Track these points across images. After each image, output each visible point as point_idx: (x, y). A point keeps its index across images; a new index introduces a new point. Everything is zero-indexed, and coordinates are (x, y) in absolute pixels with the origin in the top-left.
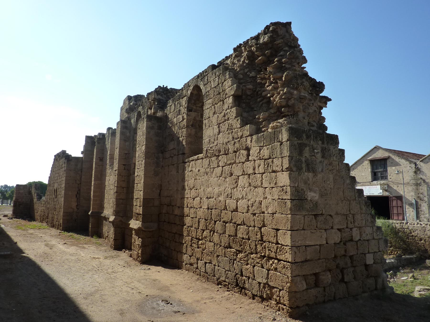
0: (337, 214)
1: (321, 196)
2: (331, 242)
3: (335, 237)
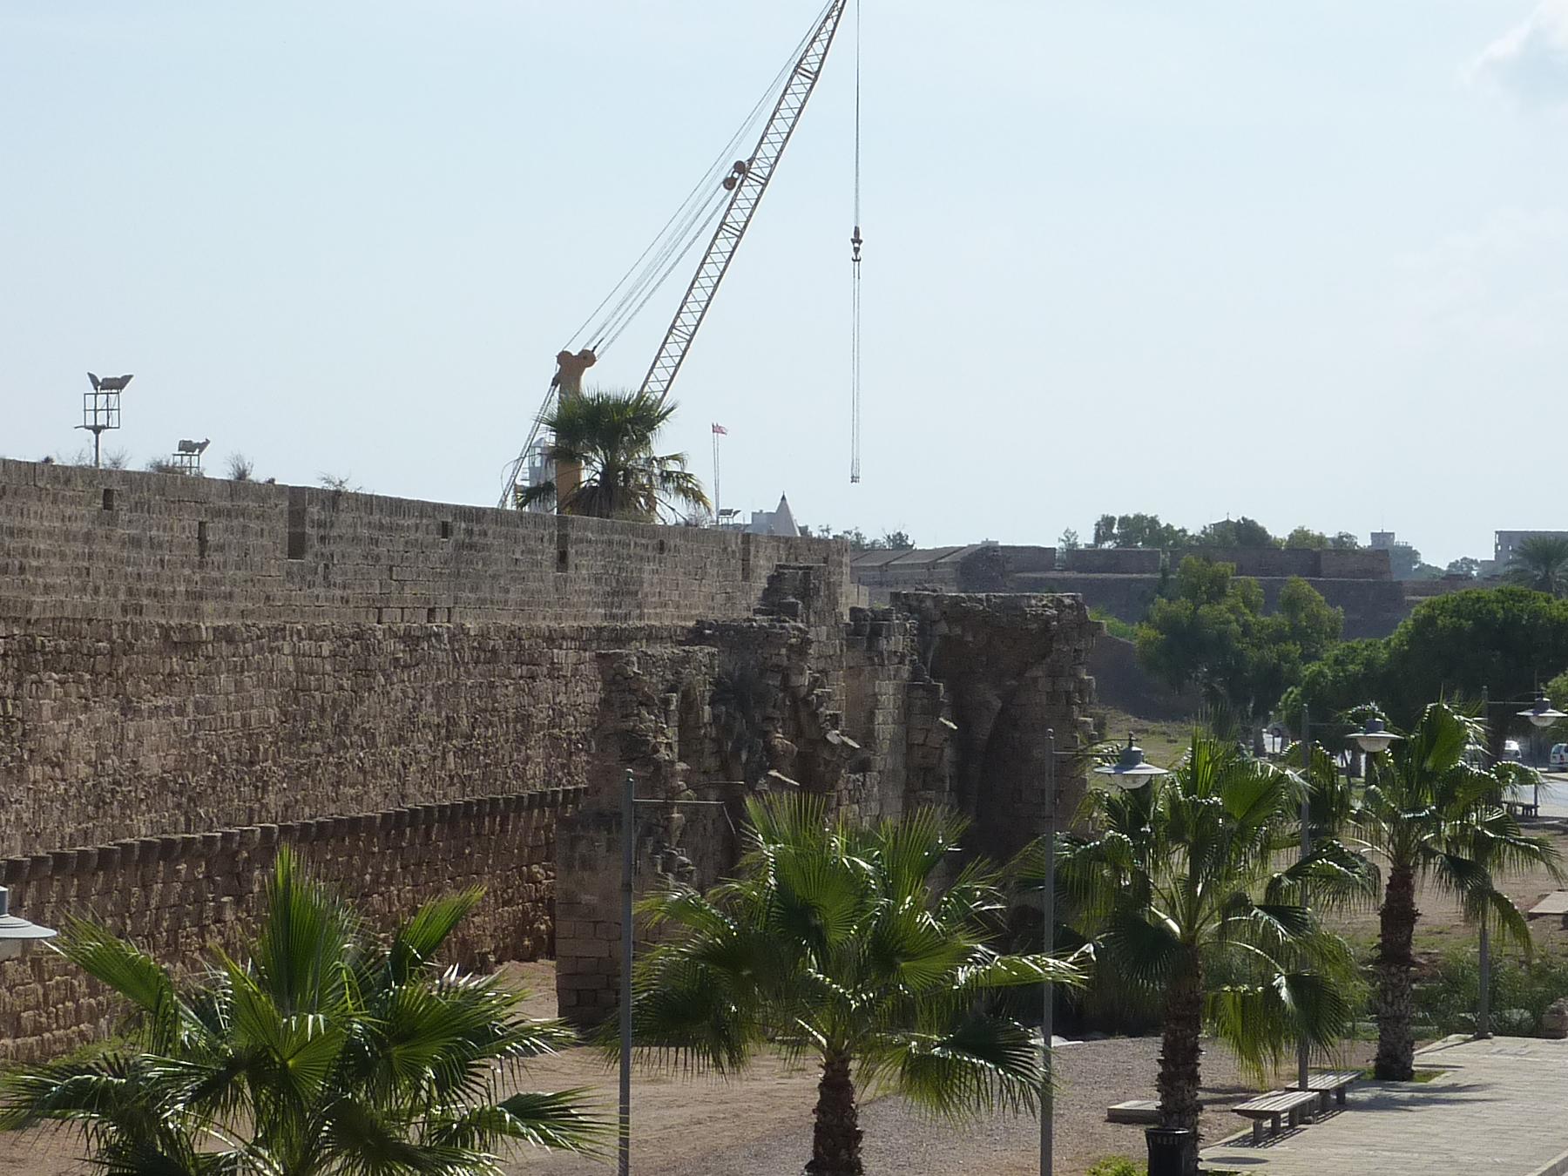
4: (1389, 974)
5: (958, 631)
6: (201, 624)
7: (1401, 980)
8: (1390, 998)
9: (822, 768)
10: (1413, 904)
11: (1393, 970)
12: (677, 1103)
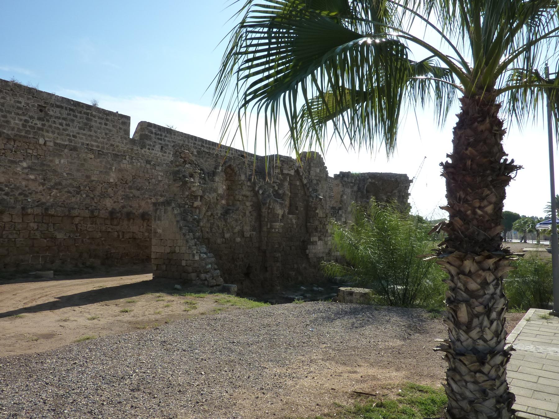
0: (169, 239)
1: (163, 231)
2: (166, 252)
3: (168, 250)
4: (461, 272)
5: (374, 181)
6: (351, 224)
7: (485, 284)
8: (463, 314)
9: (310, 204)
10: (501, 139)
11: (469, 265)
12: (230, 304)
